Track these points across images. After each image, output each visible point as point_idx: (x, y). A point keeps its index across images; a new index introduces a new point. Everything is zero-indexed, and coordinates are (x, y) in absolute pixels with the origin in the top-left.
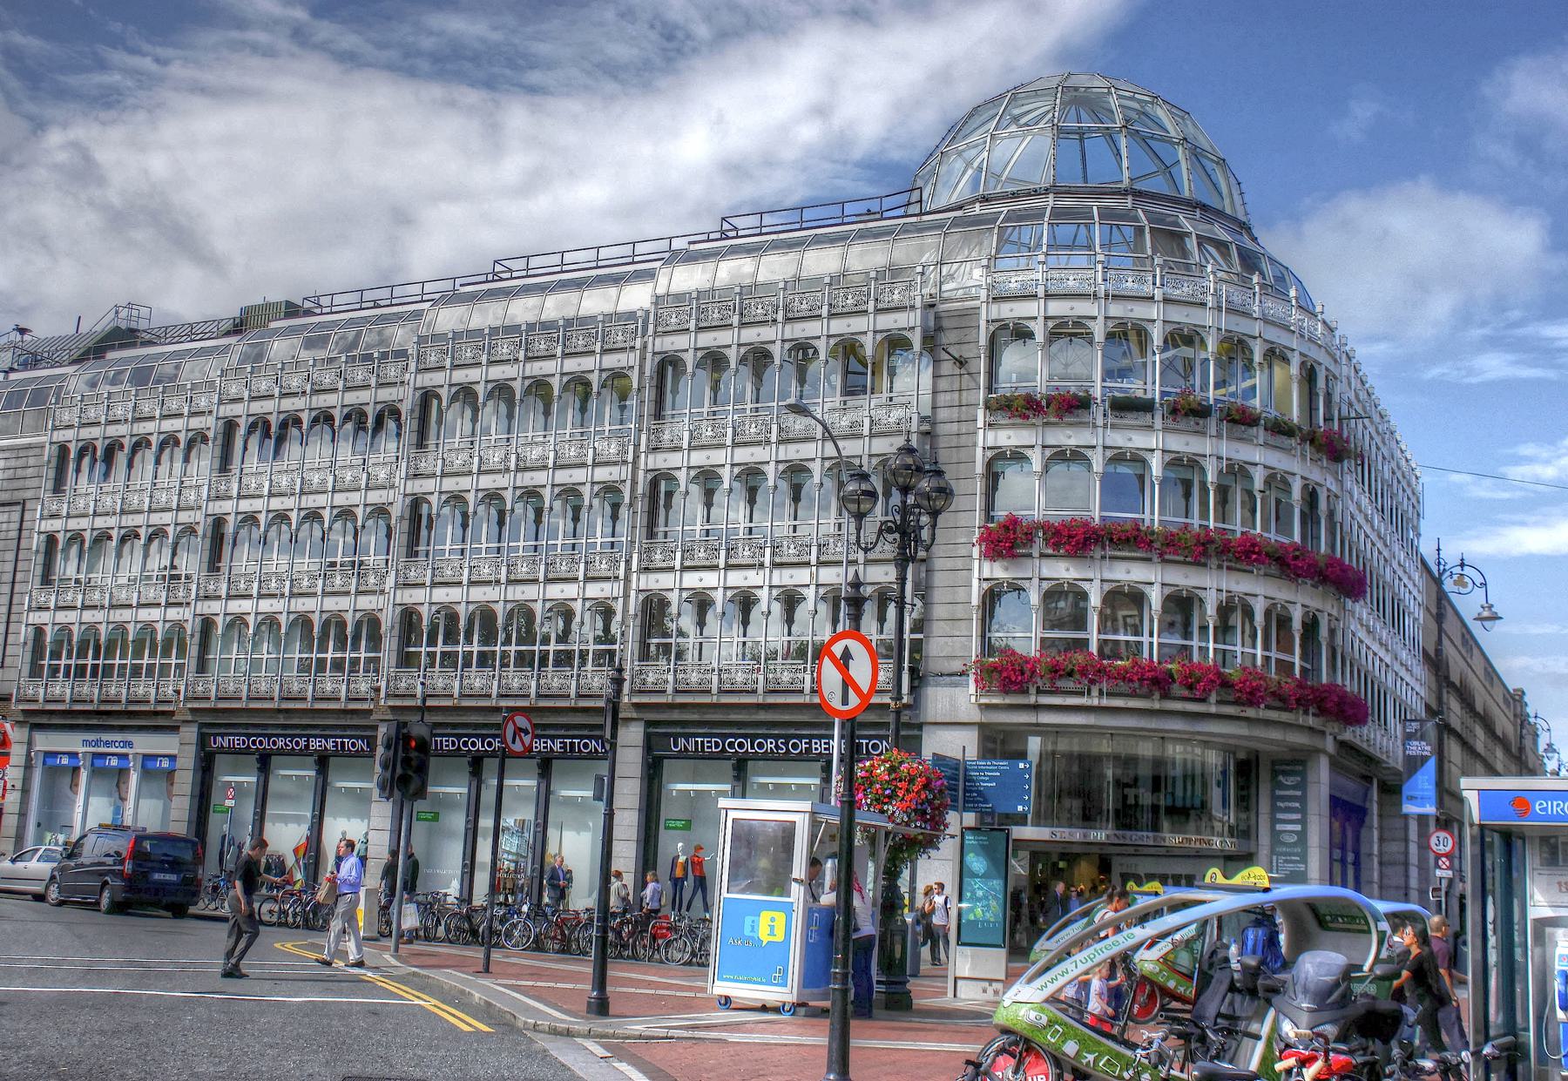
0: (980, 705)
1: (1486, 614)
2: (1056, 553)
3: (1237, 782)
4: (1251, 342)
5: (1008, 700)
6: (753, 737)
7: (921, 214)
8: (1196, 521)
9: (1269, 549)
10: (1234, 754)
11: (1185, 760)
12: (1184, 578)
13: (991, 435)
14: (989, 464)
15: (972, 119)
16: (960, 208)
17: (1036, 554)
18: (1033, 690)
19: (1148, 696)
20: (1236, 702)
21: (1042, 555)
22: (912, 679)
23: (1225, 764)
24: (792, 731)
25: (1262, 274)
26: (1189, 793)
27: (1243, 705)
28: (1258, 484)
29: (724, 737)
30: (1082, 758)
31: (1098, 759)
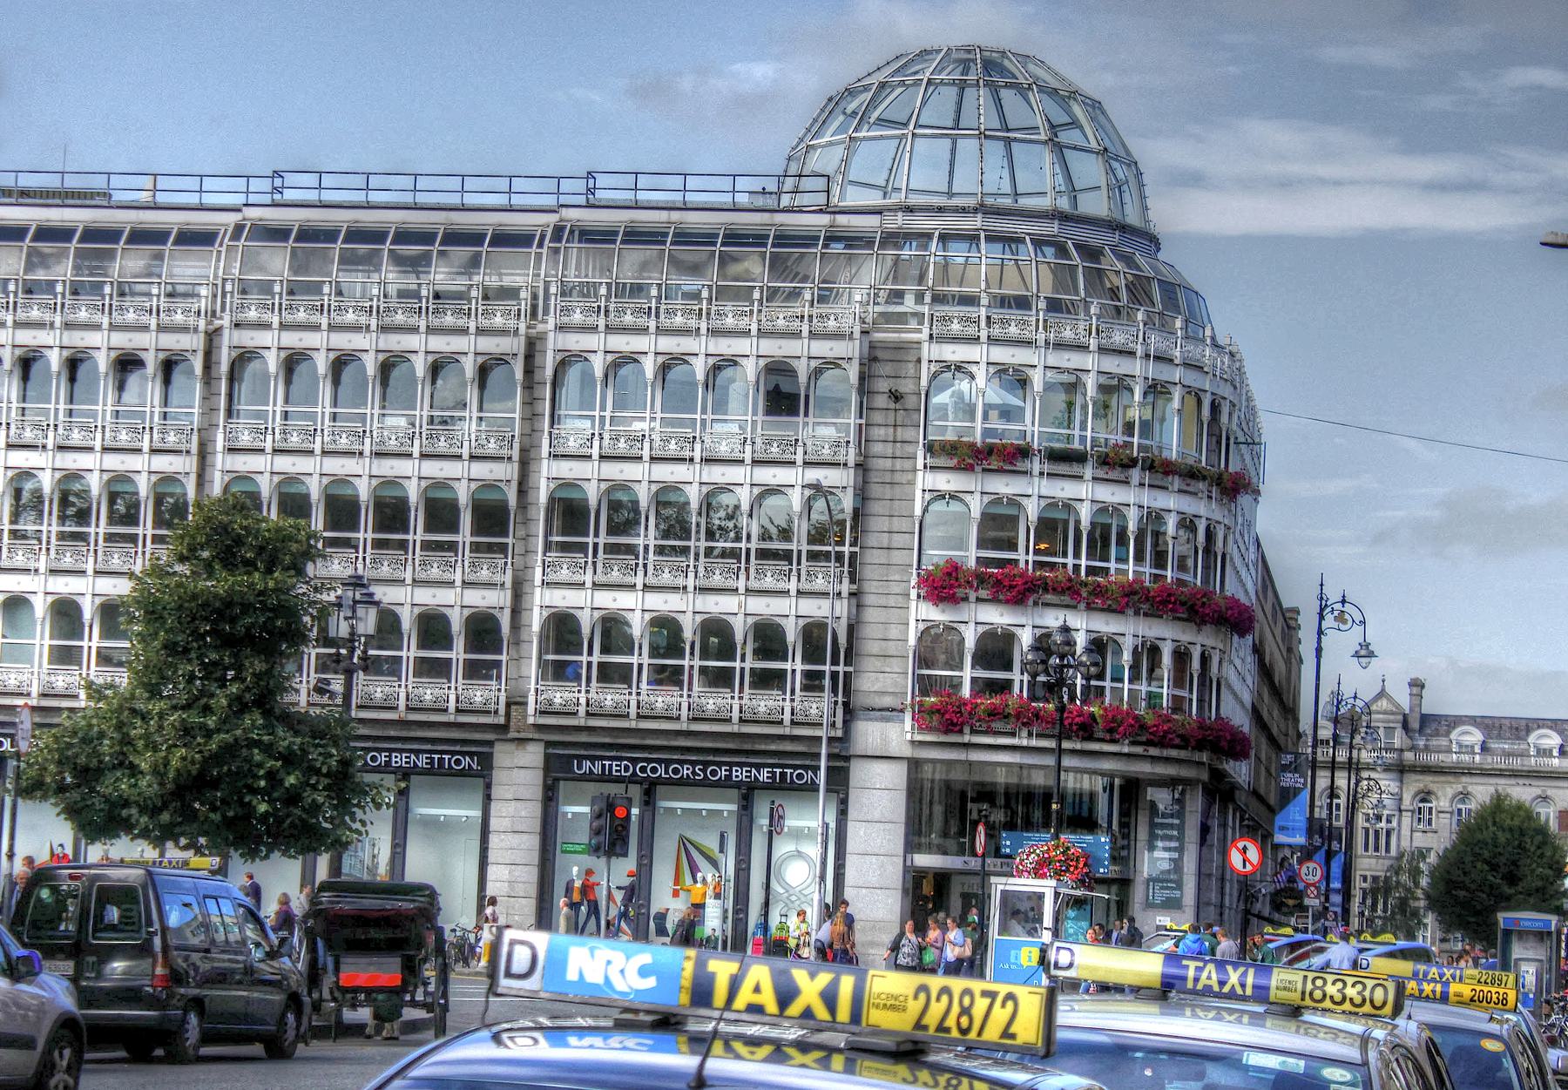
1: (1363, 652)
6: (668, 762)
12: (1106, 625)
24: (711, 758)
29: (634, 761)
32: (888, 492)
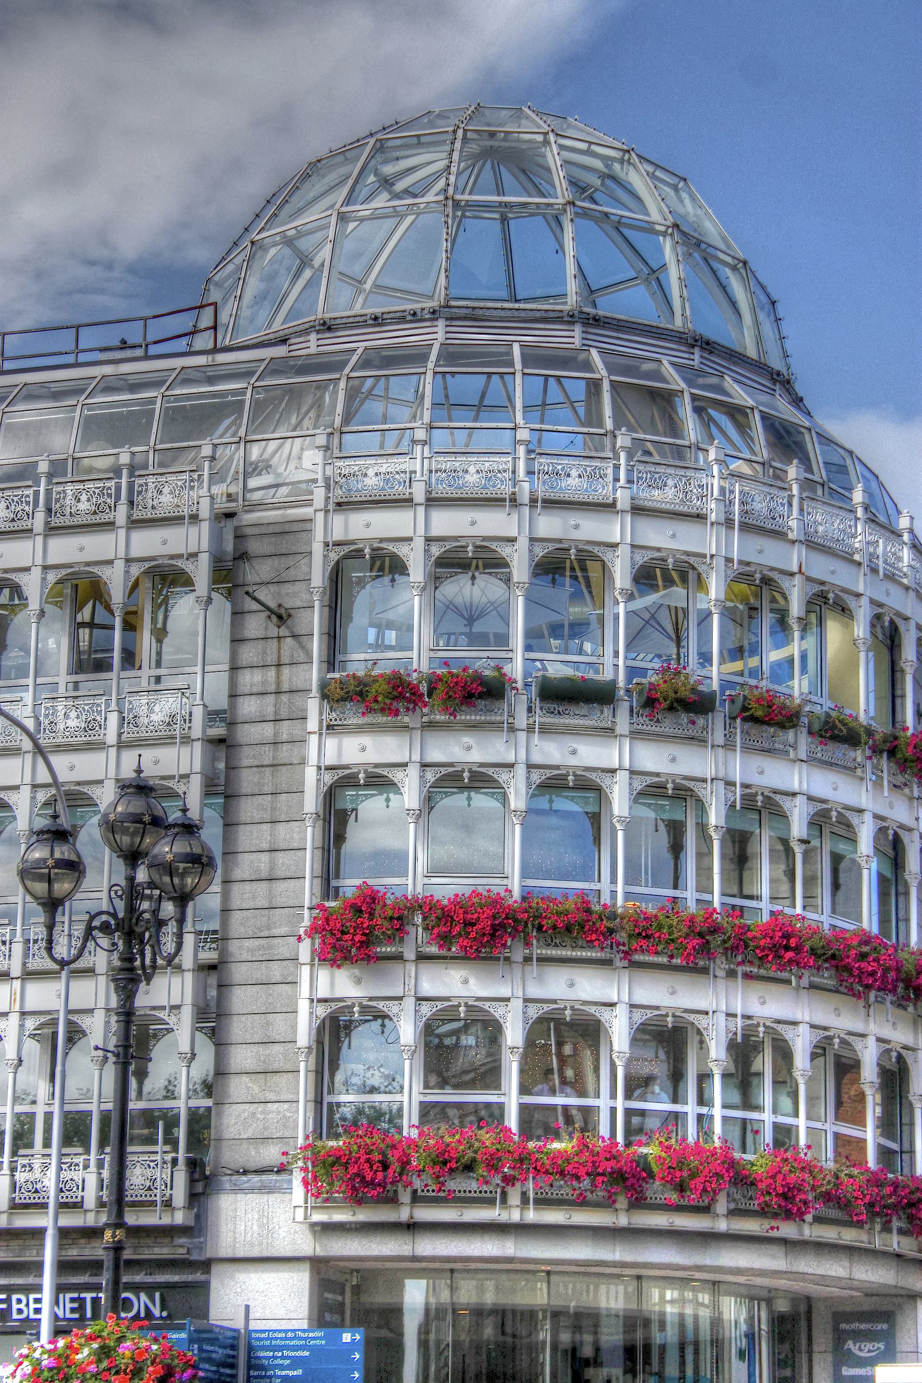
0: (313, 1225)
2: (444, 952)
3: (773, 1354)
4: (785, 583)
5: (363, 1215)
7: (215, 350)
8: (690, 895)
9: (816, 941)
10: (769, 1301)
11: (682, 1316)
13: (331, 743)
14: (330, 796)
15: (307, 185)
16: (284, 341)
17: (410, 955)
18: (405, 1197)
19: (608, 1203)
20: (762, 1213)
21: (422, 957)
22: (192, 1181)
23: (750, 1320)
25: (806, 462)
26: (689, 1371)
27: (775, 1216)
28: (798, 828)
30: (502, 1314)
31: (530, 1316)
32: (268, 780)
